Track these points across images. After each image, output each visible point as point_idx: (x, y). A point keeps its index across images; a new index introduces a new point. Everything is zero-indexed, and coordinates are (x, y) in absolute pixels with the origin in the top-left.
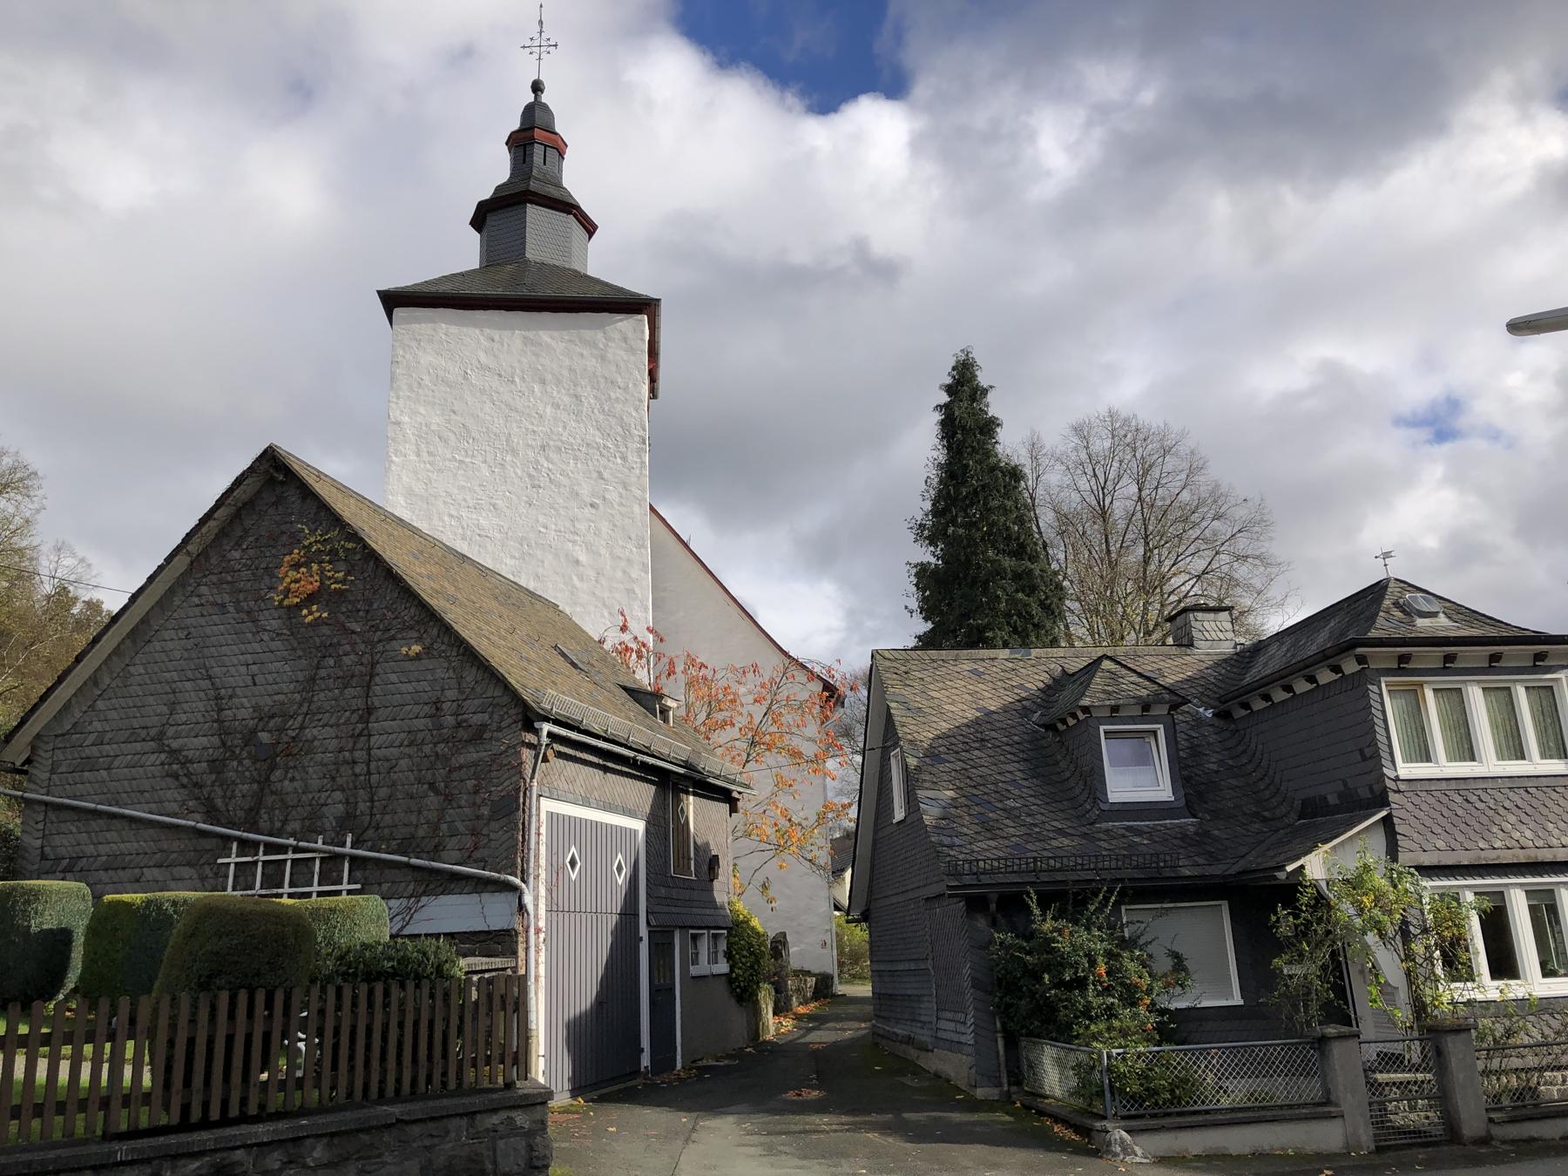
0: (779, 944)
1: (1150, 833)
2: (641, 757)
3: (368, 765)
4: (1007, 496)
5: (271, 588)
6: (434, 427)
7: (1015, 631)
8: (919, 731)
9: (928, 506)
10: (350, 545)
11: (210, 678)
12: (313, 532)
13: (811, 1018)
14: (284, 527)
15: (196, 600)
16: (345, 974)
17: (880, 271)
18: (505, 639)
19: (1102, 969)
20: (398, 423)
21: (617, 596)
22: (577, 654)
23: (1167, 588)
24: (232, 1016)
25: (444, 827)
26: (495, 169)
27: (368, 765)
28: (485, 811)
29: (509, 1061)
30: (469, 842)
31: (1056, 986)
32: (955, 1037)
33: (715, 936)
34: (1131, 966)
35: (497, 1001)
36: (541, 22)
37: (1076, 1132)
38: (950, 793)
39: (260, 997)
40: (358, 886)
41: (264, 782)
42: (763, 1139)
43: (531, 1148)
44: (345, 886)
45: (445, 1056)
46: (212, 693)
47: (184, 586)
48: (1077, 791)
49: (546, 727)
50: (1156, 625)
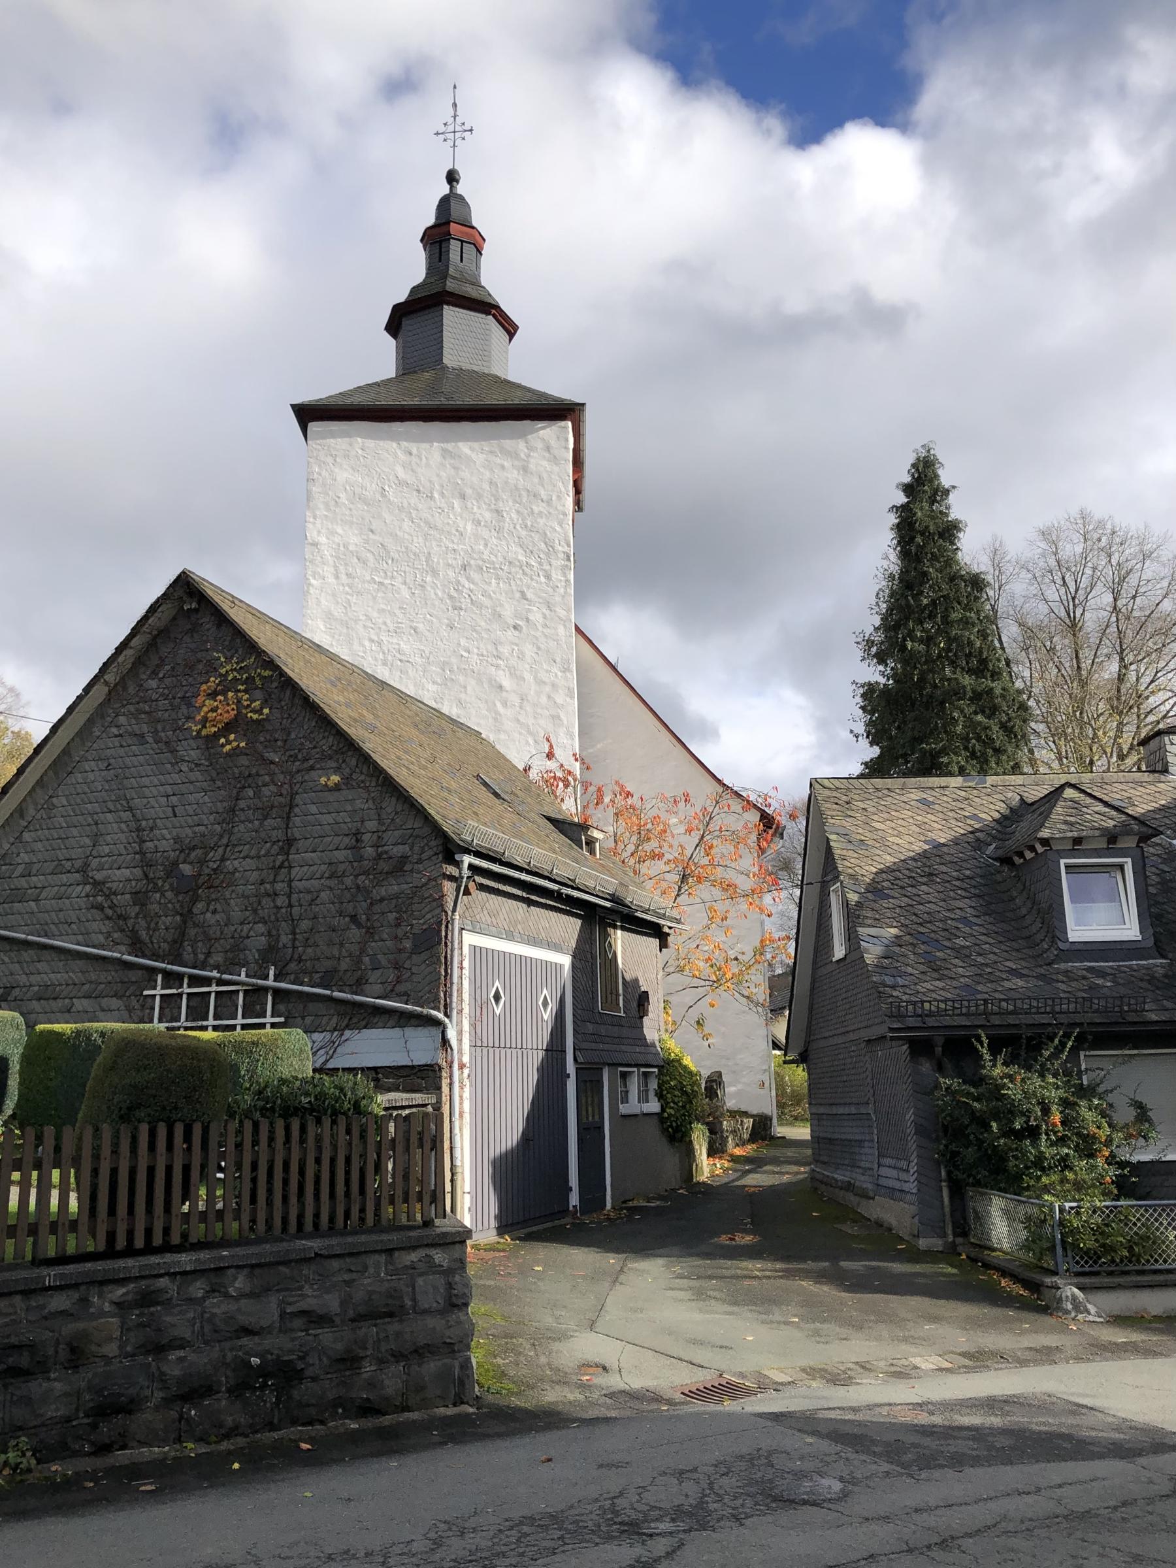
0: (715, 1083)
1: (1113, 975)
2: (565, 890)
3: (289, 897)
4: (968, 608)
5: (189, 718)
6: (351, 548)
7: (973, 755)
8: (859, 867)
9: (877, 621)
10: (267, 673)
11: (131, 809)
12: (229, 659)
13: (747, 1160)
14: (199, 655)
15: (115, 731)
16: (263, 1109)
17: (882, 319)
18: (425, 768)
19: (1056, 1118)
20: (315, 544)
21: (542, 722)
22: (498, 784)
23: (1145, 707)
24: (152, 1147)
25: (366, 960)
26: (412, 270)
27: (289, 897)
28: (408, 944)
29: (427, 1198)
30: (391, 975)
31: (1005, 1134)
32: (897, 1185)
33: (646, 1074)
34: (1089, 1115)
35: (414, 1139)
36: (455, 105)
37: (1025, 1287)
38: (894, 931)
39: (179, 1129)
40: (282, 1020)
41: (187, 915)
42: (695, 1283)
43: (450, 1286)
44: (269, 1019)
45: (362, 1191)
46: (133, 825)
47: (103, 717)
48: (1034, 929)
49: (467, 859)
50: (1131, 748)
